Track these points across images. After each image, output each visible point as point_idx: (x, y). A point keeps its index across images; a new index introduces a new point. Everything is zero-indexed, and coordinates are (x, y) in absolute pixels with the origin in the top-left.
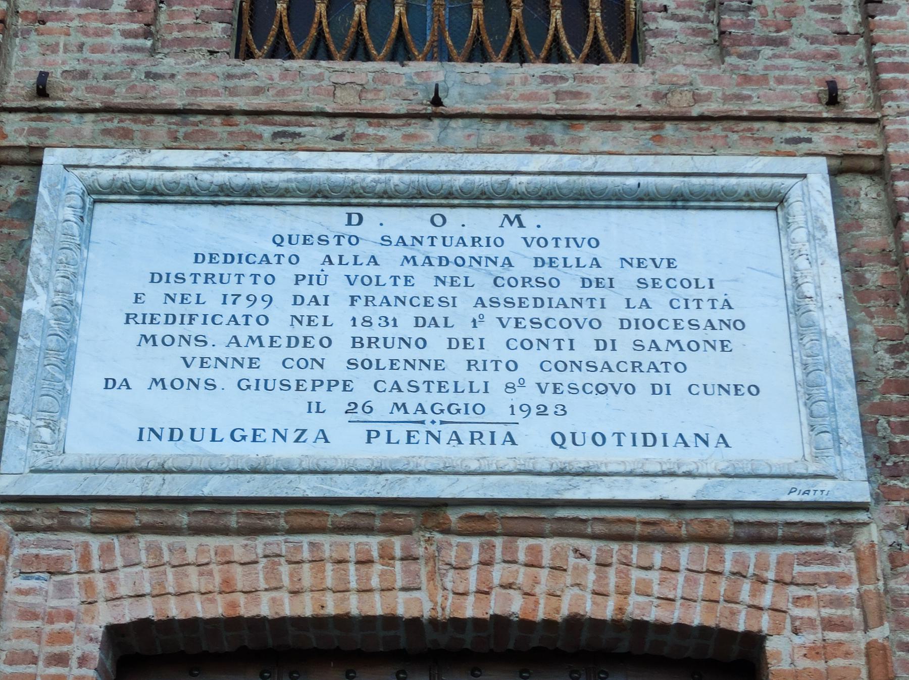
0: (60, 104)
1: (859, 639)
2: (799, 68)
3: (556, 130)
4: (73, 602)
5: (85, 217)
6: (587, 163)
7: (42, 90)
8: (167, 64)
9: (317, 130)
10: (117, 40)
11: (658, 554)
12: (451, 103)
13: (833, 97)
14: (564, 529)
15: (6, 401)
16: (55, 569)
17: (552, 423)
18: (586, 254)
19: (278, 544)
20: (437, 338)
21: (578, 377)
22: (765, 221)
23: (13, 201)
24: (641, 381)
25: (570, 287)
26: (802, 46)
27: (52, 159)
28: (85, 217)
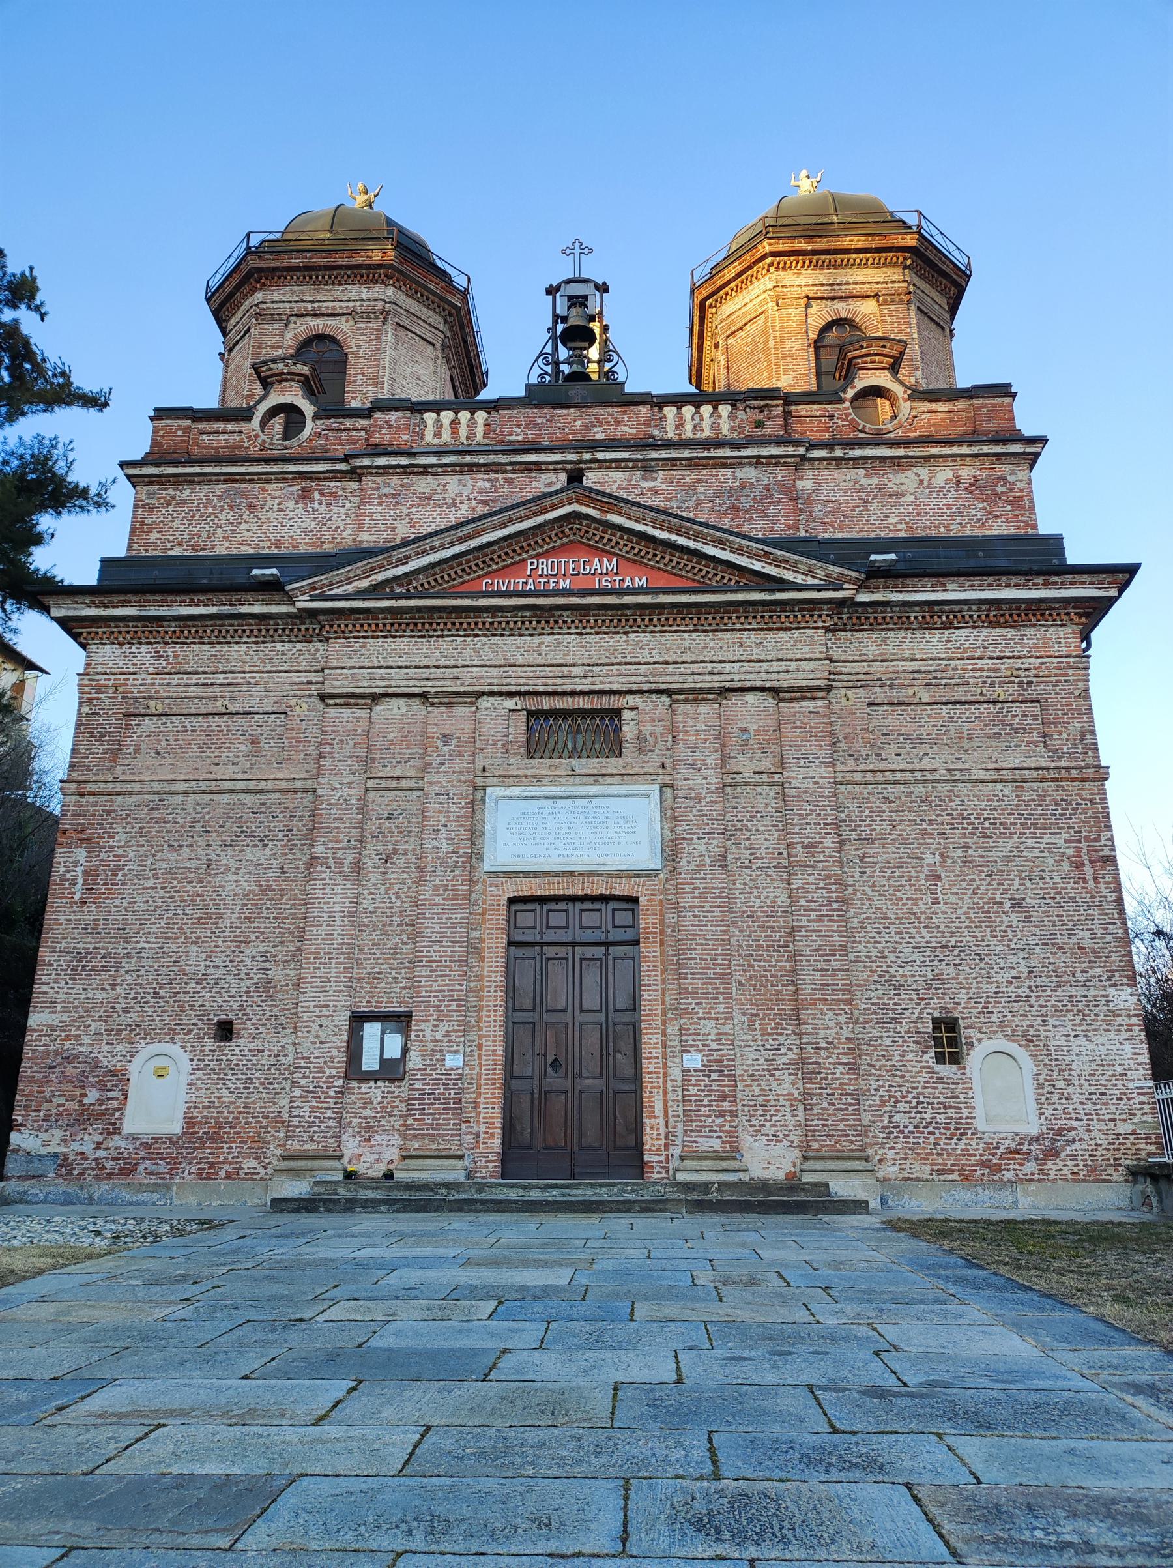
0: (510, 703)
1: (658, 898)
2: (656, 758)
3: (600, 778)
4: (501, 893)
5: (497, 804)
6: (606, 787)
7: (484, 770)
8: (512, 760)
9: (546, 780)
10: (500, 755)
11: (618, 880)
12: (578, 771)
13: (663, 767)
14: (599, 876)
15: (1128, 576)
16: (496, 886)
17: (598, 851)
18: (606, 810)
19: (542, 879)
20: (573, 831)
21: (603, 841)
22: (646, 800)
23: (597, 437)
24: (617, 841)
25: (602, 819)
26: (657, 752)
27: (489, 790)
28: (497, 804)
